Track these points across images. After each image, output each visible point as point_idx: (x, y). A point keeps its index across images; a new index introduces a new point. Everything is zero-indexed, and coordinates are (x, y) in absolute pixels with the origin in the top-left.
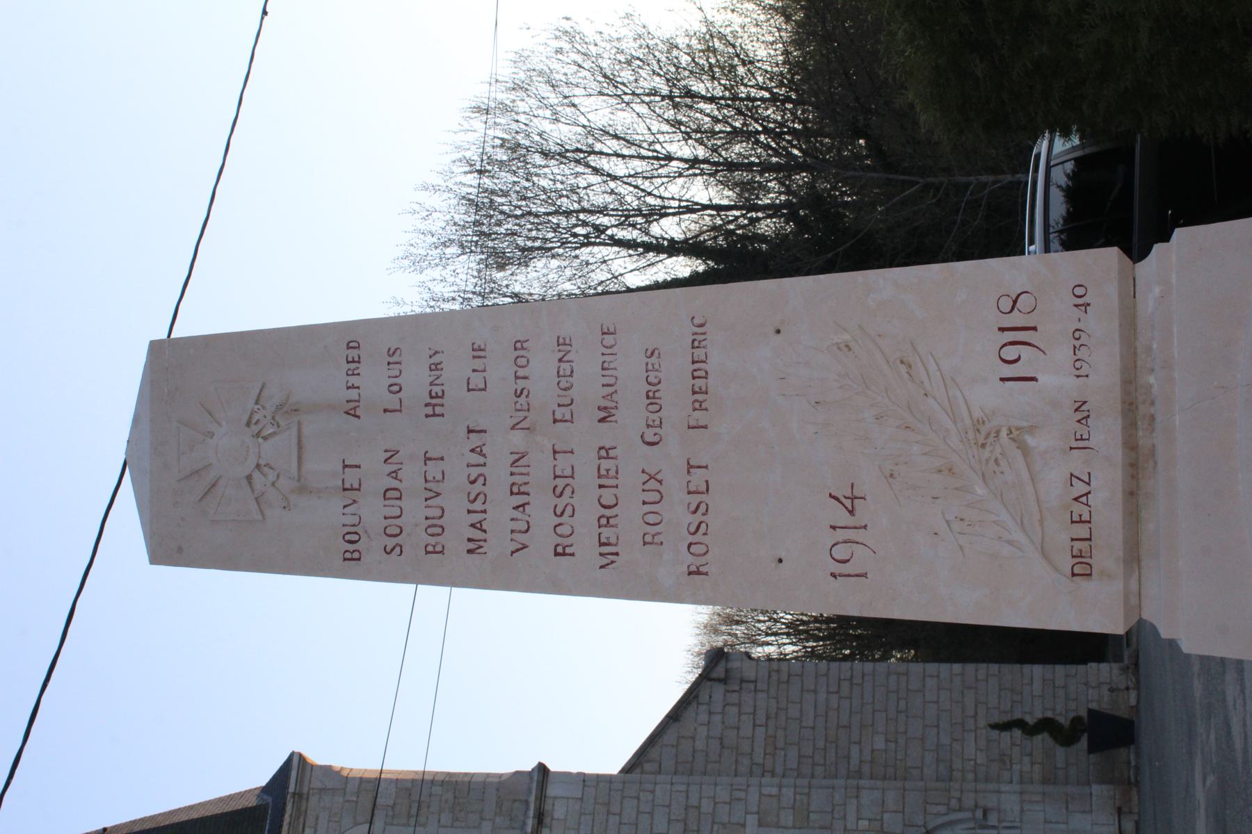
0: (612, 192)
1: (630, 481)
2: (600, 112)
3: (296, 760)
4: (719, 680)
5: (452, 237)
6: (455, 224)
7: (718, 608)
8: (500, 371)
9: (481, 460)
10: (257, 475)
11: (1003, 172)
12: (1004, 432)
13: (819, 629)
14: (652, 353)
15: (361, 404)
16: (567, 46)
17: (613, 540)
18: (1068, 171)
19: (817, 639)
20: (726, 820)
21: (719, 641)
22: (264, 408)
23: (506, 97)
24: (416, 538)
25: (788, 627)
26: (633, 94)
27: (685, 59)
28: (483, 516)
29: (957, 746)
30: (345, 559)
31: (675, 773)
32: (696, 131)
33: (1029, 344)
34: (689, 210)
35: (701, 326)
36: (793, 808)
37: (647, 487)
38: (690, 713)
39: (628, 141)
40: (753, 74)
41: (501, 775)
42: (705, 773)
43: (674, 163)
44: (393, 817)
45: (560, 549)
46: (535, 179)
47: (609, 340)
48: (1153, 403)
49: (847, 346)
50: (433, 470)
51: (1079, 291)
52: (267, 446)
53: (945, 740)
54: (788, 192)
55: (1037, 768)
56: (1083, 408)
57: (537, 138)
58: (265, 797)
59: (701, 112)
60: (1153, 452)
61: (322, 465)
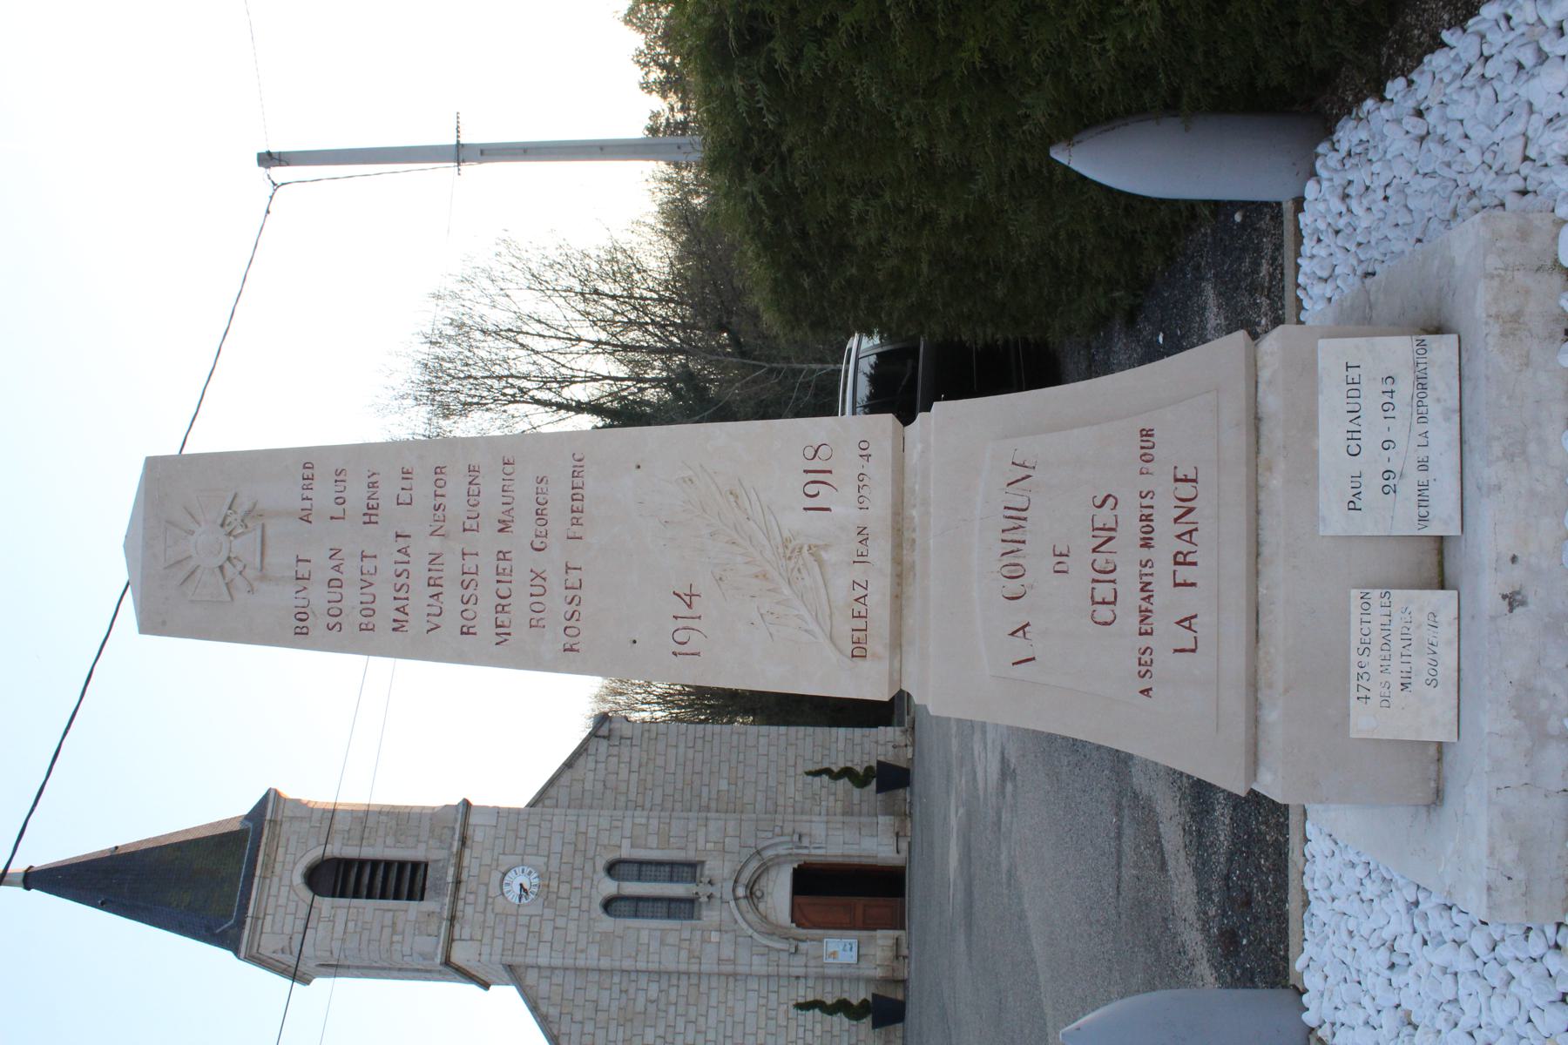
0: (534, 363)
1: (521, 577)
2: (530, 302)
3: (272, 795)
4: (604, 737)
5: (409, 392)
6: (412, 382)
7: (606, 682)
8: (423, 490)
9: (406, 558)
10: (228, 566)
11: (828, 363)
12: (806, 548)
13: (682, 700)
14: (542, 480)
15: (313, 512)
16: (504, 251)
17: (506, 623)
18: (872, 363)
19: (680, 707)
20: (606, 842)
21: (606, 708)
22: (235, 512)
23: (457, 288)
24: (353, 618)
25: (658, 698)
26: (554, 290)
27: (594, 267)
28: (405, 602)
29: (781, 788)
30: (296, 634)
31: (569, 807)
32: (600, 320)
33: (825, 483)
34: (594, 380)
35: (580, 460)
36: (658, 834)
37: (534, 583)
38: (581, 761)
39: (547, 325)
40: (645, 280)
41: (434, 808)
42: (591, 807)
43: (583, 343)
44: (349, 839)
45: (465, 630)
46: (475, 350)
47: (509, 469)
48: (914, 530)
49: (690, 480)
50: (368, 565)
51: (864, 445)
52: (236, 543)
53: (772, 783)
54: (667, 369)
55: (839, 804)
56: (864, 532)
57: (479, 320)
58: (247, 823)
59: (605, 306)
60: (913, 566)
61: (281, 560)
